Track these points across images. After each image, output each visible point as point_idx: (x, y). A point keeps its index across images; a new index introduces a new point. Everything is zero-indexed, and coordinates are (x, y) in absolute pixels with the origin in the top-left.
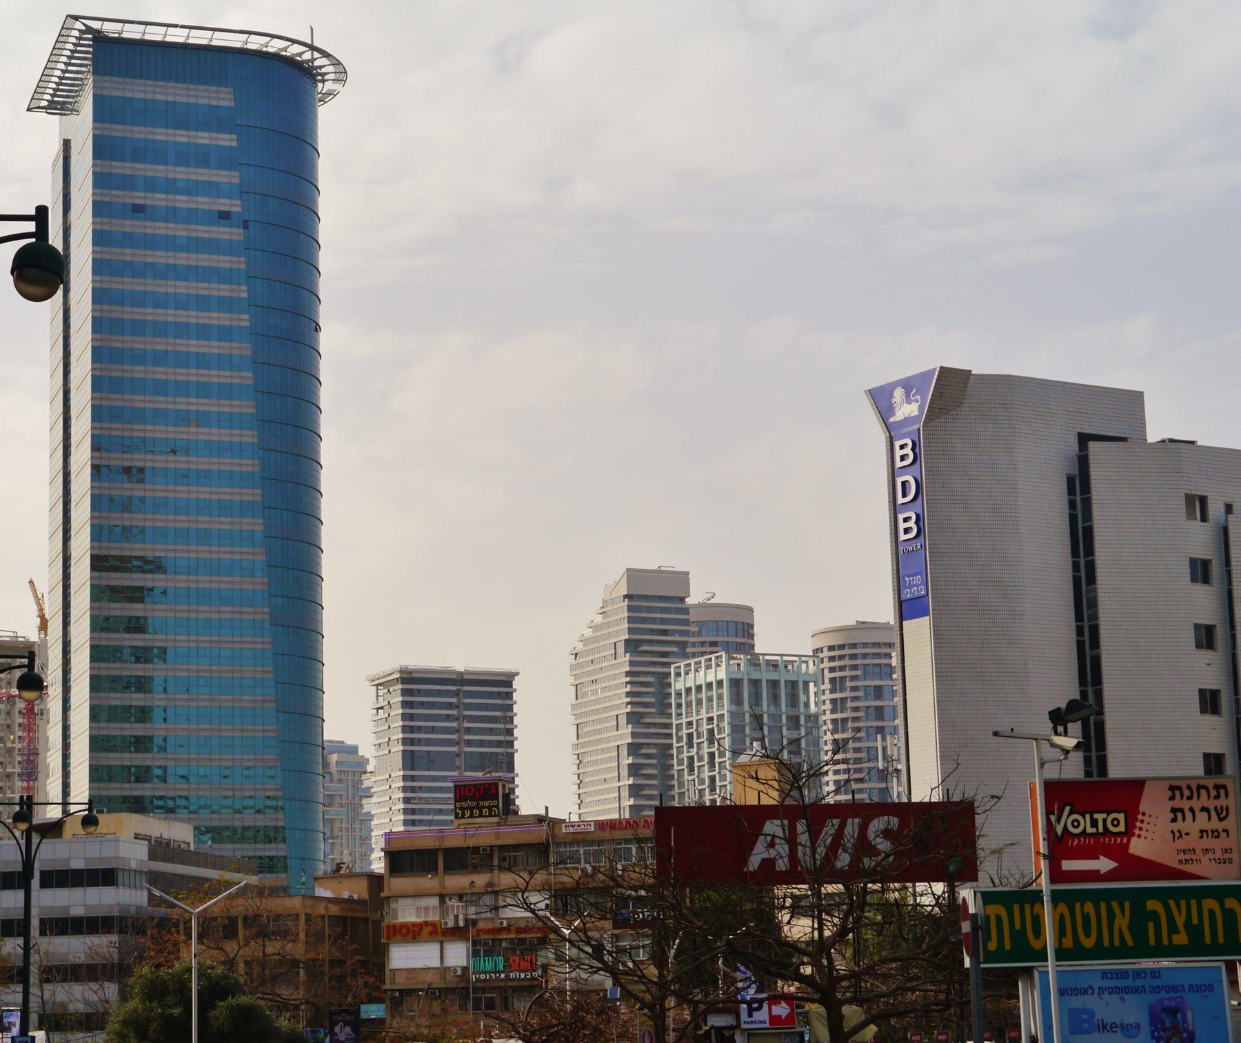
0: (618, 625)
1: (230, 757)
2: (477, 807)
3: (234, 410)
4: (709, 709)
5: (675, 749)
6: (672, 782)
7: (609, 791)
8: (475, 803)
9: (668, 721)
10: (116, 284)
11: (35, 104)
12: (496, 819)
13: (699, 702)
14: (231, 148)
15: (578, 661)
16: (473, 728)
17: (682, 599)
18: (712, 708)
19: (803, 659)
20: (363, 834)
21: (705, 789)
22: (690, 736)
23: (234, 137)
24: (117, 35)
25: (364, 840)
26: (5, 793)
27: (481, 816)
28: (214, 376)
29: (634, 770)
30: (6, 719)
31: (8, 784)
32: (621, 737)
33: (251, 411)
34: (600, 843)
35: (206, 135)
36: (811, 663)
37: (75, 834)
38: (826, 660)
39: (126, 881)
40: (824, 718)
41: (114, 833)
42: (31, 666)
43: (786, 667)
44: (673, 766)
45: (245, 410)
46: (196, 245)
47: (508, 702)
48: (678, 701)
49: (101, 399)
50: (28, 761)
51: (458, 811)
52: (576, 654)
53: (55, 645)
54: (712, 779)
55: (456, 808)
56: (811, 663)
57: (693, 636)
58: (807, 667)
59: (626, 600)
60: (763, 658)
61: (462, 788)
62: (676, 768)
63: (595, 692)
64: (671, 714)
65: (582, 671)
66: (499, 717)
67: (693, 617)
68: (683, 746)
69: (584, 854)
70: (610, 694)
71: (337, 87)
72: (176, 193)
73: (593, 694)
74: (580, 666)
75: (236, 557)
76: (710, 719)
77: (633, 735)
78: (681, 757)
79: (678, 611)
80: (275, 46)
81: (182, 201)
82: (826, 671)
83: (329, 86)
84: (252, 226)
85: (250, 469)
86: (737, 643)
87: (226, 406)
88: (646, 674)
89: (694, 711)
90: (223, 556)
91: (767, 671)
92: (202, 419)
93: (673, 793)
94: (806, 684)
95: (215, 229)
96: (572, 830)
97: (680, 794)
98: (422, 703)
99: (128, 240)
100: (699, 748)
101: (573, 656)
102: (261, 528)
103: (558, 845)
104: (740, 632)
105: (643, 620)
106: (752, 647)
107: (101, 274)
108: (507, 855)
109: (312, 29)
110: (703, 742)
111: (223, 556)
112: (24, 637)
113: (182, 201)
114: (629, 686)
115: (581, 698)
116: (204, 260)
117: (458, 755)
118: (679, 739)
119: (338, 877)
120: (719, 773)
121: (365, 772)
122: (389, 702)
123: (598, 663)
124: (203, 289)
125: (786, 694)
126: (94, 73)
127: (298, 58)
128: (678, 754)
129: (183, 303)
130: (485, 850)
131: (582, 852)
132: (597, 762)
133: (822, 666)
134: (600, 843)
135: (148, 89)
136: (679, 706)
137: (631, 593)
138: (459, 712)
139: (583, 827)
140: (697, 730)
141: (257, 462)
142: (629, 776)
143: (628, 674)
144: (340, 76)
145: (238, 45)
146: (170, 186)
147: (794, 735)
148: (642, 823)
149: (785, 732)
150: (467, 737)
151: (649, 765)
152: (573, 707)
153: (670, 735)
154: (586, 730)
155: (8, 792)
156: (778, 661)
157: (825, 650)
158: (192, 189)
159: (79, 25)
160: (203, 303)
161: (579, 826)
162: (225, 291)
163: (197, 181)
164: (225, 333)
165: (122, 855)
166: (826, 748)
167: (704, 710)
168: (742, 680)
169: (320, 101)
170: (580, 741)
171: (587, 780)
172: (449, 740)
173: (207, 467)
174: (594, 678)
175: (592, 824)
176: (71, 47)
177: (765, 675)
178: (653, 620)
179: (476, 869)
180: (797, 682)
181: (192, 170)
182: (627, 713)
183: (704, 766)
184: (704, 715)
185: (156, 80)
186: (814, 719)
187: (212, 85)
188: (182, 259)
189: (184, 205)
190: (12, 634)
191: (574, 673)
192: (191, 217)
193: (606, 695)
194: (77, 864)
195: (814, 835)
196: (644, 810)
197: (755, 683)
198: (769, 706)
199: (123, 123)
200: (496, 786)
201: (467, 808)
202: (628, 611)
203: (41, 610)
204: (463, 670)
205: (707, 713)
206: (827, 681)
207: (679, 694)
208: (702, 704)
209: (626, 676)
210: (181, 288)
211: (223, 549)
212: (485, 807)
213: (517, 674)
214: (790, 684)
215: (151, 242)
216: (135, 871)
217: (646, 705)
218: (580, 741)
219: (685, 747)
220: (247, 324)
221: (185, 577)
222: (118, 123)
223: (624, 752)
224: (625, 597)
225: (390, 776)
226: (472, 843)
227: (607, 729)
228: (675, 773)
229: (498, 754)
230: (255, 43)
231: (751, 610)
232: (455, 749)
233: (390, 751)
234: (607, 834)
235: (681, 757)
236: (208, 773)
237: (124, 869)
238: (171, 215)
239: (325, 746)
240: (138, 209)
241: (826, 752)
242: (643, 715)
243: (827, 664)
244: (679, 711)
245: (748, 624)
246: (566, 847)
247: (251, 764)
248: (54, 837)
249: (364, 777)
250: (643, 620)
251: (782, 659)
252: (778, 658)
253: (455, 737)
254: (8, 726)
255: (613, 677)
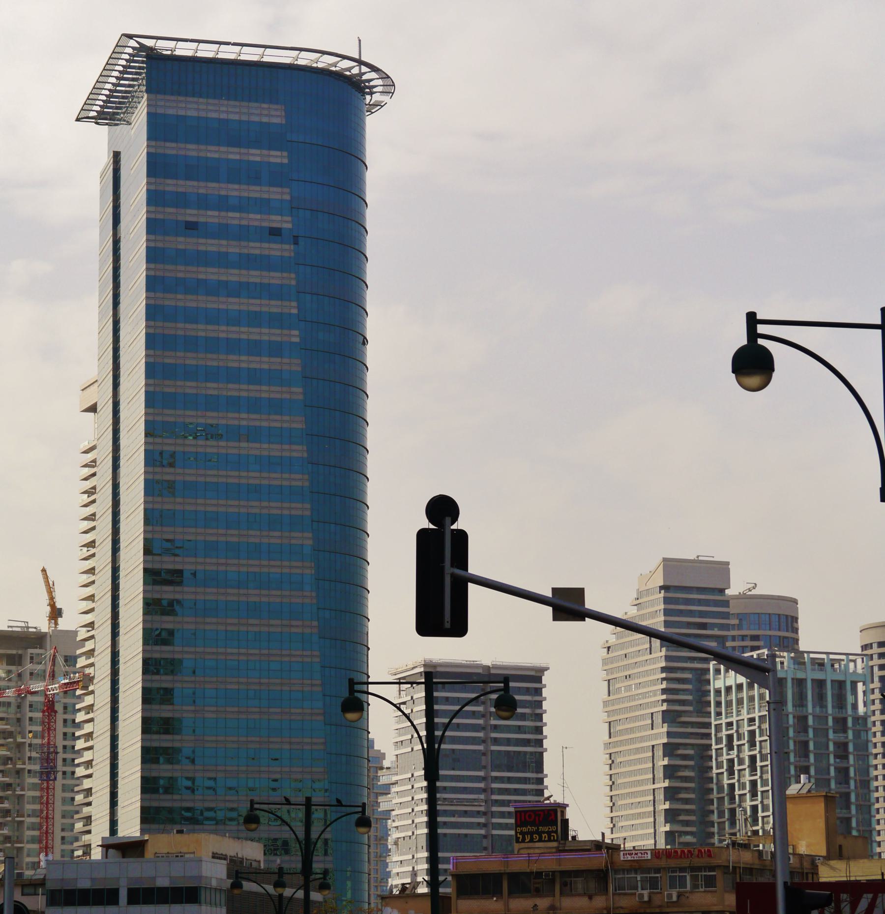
0: (653, 618)
1: (279, 769)
2: (537, 832)
3: (285, 425)
4: (750, 710)
5: (714, 751)
6: (711, 786)
7: (643, 793)
8: (535, 829)
9: (706, 720)
10: (169, 301)
11: (84, 114)
12: (555, 844)
13: (740, 702)
14: (282, 164)
15: (611, 655)
16: (500, 725)
17: (722, 591)
18: (754, 708)
19: (851, 657)
20: (378, 834)
21: (745, 794)
22: (730, 738)
23: (285, 154)
24: (169, 53)
25: (380, 840)
26: (15, 791)
27: (540, 840)
28: (265, 392)
29: (670, 772)
30: (16, 713)
31: (18, 781)
32: (656, 736)
33: (300, 426)
34: (658, 871)
35: (258, 152)
36: (859, 661)
37: (156, 853)
38: (876, 657)
39: (208, 900)
40: (873, 719)
41: (194, 853)
42: (363, 812)
43: (833, 666)
44: (712, 768)
45: (294, 425)
46: (248, 262)
47: (537, 698)
48: (718, 699)
49: (154, 414)
50: (48, 760)
51: (518, 836)
52: (609, 648)
53: (103, 654)
54: (754, 784)
55: (516, 833)
56: (859, 661)
57: (733, 629)
58: (855, 666)
59: (663, 591)
60: (808, 656)
61: (523, 814)
62: (715, 771)
63: (628, 688)
64: (710, 713)
65: (615, 665)
66: (528, 714)
67: (733, 609)
68: (722, 749)
69: (641, 881)
70: (645, 690)
71: (385, 98)
72: (228, 210)
73: (626, 691)
74: (612, 660)
75: (285, 571)
76: (752, 720)
77: (669, 734)
78: (720, 759)
79: (717, 603)
80: (324, 62)
81: (234, 218)
82: (876, 669)
83: (376, 97)
84: (301, 242)
85: (299, 484)
86: (780, 637)
87: (276, 422)
88: (683, 669)
89: (734, 711)
90: (272, 570)
91: (813, 670)
92: (252, 434)
93: (711, 797)
94: (854, 684)
95: (266, 245)
96: (629, 858)
97: (718, 799)
98: (447, 699)
99: (182, 257)
100: (739, 751)
101: (606, 650)
102: (310, 542)
103: (616, 871)
104: (783, 625)
105: (681, 613)
106: (796, 641)
107: (154, 291)
108: (568, 880)
109: (360, 41)
110: (744, 744)
111: (272, 570)
112: (35, 628)
113: (234, 218)
114: (665, 682)
115: (614, 694)
116: (255, 276)
117: (484, 754)
118: (719, 741)
119: (404, 897)
120: (761, 777)
121: (382, 768)
122: (412, 698)
123: (633, 658)
124: (255, 305)
125: (833, 695)
126: (147, 91)
127: (348, 73)
128: (717, 756)
129: (235, 320)
130: (547, 875)
131: (639, 879)
132: (630, 763)
133: (871, 663)
134: (658, 871)
135: (201, 107)
136: (718, 704)
137: (668, 584)
138: (485, 709)
139: (640, 855)
140: (737, 731)
141: (306, 477)
142: (665, 778)
143: (663, 670)
144: (387, 89)
145: (288, 61)
146: (223, 204)
147: (841, 737)
148: (696, 852)
149: (831, 735)
150: (494, 735)
151: (686, 767)
152: (606, 703)
153: (708, 736)
154: (618, 728)
155: (18, 789)
156: (824, 659)
157: (875, 646)
158: (243, 206)
159: (132, 43)
160: (255, 319)
161: (636, 854)
162: (274, 306)
163: (249, 198)
164: (276, 350)
165: (204, 874)
166: (874, 751)
167: (744, 711)
168: (786, 679)
169: (367, 111)
170: (612, 740)
171: (620, 781)
172: (474, 738)
173: (257, 482)
174: (627, 673)
175: (649, 852)
176: (124, 63)
177: (811, 675)
178: (691, 613)
179: (538, 893)
180: (844, 682)
181: (244, 187)
182: (663, 711)
183: (745, 769)
184: (745, 716)
185: (208, 97)
186: (862, 721)
187: (264, 103)
188: (234, 276)
189: (236, 222)
190: (23, 625)
191: (606, 668)
192: (243, 233)
193: (640, 691)
194: (163, 882)
195: (854, 906)
196: (680, 815)
197: (800, 683)
198: (814, 707)
199: (176, 141)
200: (555, 811)
201: (527, 833)
202: (665, 603)
203: (52, 598)
204: (490, 664)
205: (748, 713)
206: (876, 679)
207: (718, 692)
208: (743, 703)
209: (662, 672)
210: (233, 304)
211: (272, 563)
212: (544, 832)
213: (547, 669)
214: (837, 684)
215: (202, 259)
216: (216, 889)
217: (683, 703)
218: (612, 740)
219: (724, 749)
220: (297, 340)
221: (235, 591)
222: (171, 141)
223: (659, 752)
224: (661, 588)
225: (413, 775)
226: (535, 868)
227: (641, 728)
228: (714, 775)
229: (525, 753)
230: (304, 59)
231: (795, 602)
232: (481, 747)
233: (412, 749)
234: (663, 863)
235: (720, 759)
236: (257, 786)
237: (206, 887)
238: (223, 231)
239: (370, 759)
240: (191, 227)
241: (876, 755)
242: (680, 713)
243: (876, 661)
244: (718, 710)
245: (792, 617)
246: (624, 874)
247: (299, 777)
248: (138, 857)
249: (380, 773)
250: (681, 613)
251: (828, 657)
252: (824, 656)
253: (481, 734)
254: (19, 720)
255: (647, 673)
